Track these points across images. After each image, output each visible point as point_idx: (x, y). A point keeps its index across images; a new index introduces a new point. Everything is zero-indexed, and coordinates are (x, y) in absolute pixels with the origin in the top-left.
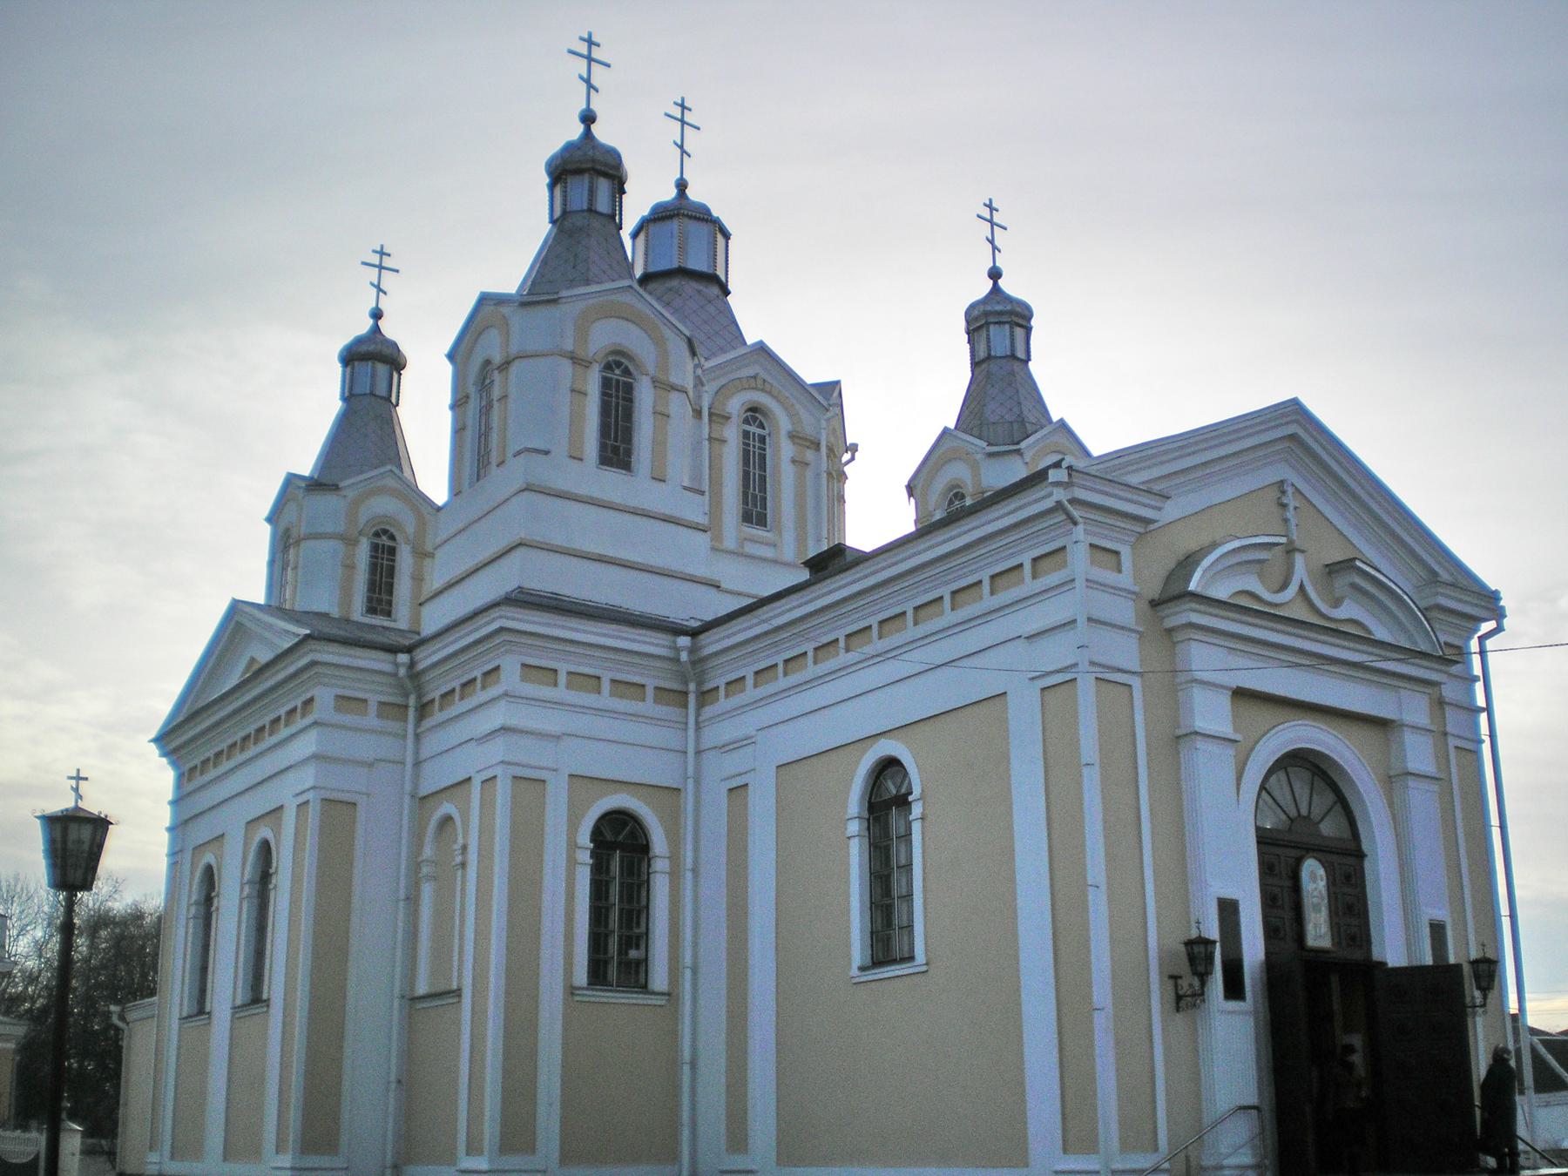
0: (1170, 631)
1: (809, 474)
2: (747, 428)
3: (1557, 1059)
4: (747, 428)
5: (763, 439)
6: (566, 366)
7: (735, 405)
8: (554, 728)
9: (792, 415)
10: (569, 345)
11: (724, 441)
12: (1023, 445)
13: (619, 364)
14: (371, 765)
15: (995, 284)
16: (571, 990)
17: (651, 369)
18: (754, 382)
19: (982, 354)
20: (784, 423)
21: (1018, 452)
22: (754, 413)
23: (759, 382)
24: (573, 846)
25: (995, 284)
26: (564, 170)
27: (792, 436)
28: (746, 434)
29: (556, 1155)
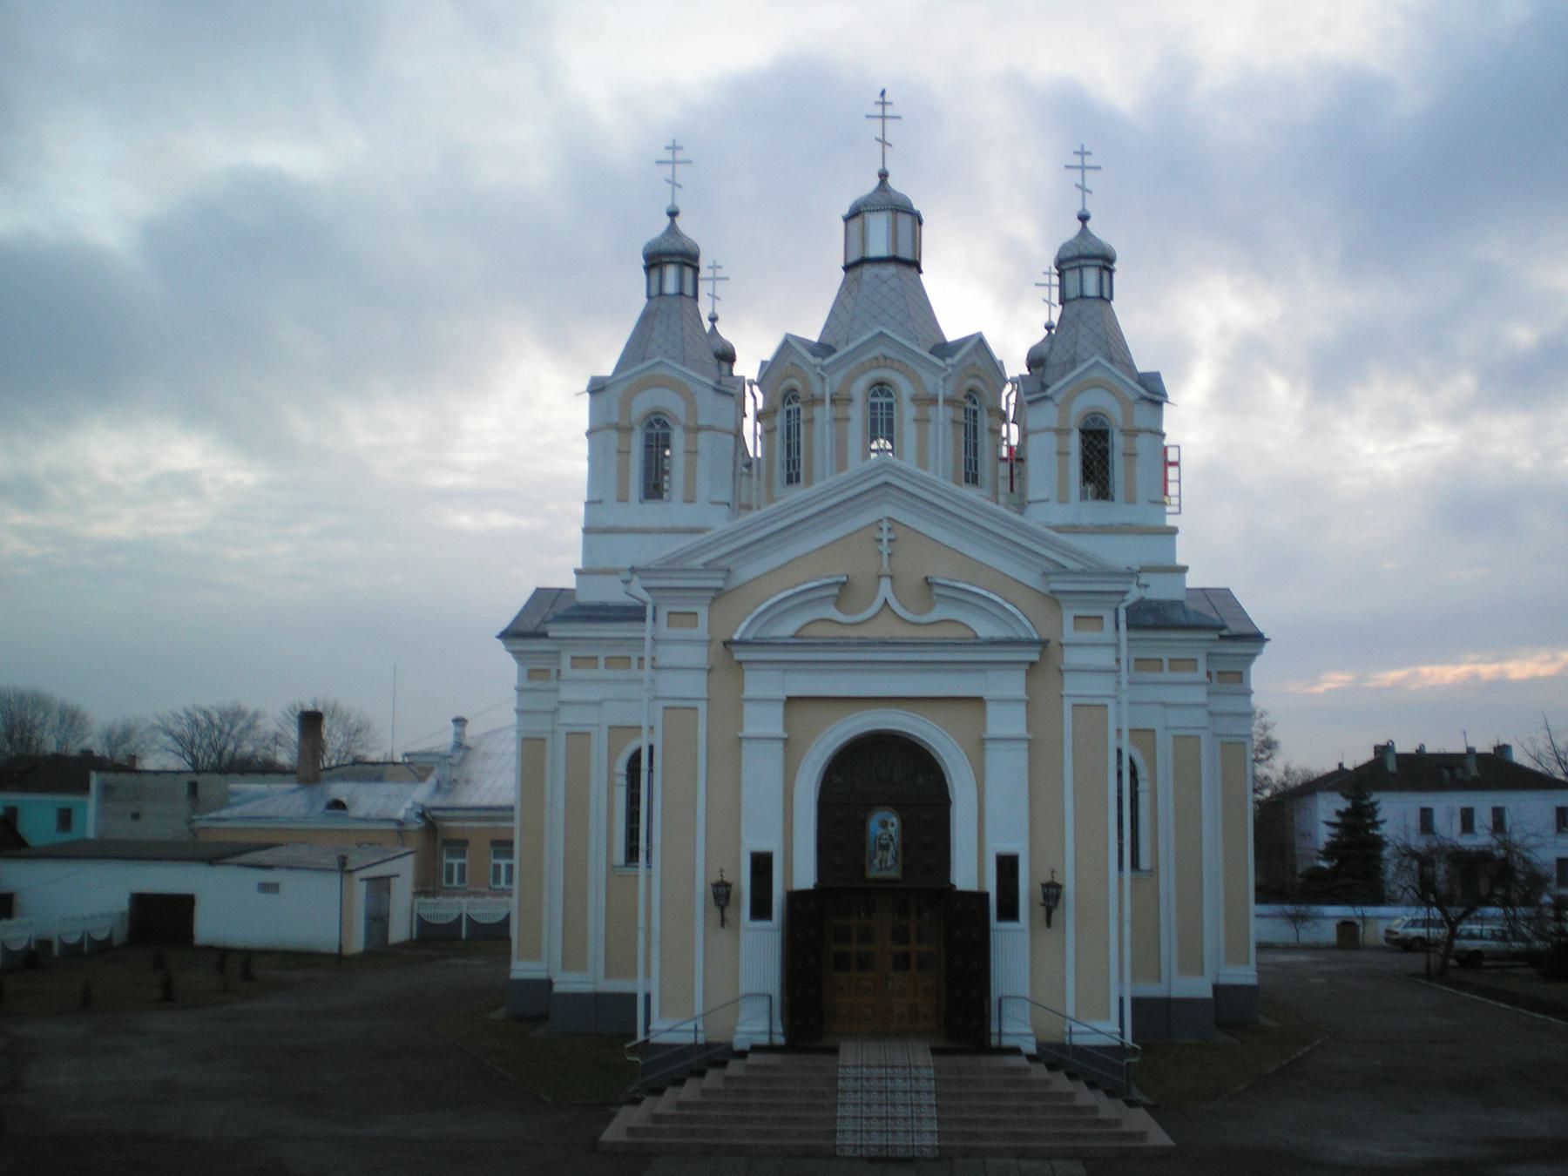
0: (740, 663)
1: (931, 428)
2: (874, 400)
3: (1133, 912)
4: (874, 400)
5: (890, 406)
6: (614, 435)
7: (860, 387)
8: (598, 698)
9: (913, 378)
10: (615, 418)
11: (848, 420)
12: (1049, 392)
13: (658, 421)
14: (599, 703)
15: (1084, 227)
16: (611, 868)
17: (682, 419)
18: (877, 363)
19: (1072, 292)
20: (905, 389)
21: (1046, 398)
22: (880, 387)
23: (881, 360)
24: (611, 774)
25: (1084, 227)
26: (655, 261)
27: (915, 400)
28: (874, 406)
29: (602, 971)
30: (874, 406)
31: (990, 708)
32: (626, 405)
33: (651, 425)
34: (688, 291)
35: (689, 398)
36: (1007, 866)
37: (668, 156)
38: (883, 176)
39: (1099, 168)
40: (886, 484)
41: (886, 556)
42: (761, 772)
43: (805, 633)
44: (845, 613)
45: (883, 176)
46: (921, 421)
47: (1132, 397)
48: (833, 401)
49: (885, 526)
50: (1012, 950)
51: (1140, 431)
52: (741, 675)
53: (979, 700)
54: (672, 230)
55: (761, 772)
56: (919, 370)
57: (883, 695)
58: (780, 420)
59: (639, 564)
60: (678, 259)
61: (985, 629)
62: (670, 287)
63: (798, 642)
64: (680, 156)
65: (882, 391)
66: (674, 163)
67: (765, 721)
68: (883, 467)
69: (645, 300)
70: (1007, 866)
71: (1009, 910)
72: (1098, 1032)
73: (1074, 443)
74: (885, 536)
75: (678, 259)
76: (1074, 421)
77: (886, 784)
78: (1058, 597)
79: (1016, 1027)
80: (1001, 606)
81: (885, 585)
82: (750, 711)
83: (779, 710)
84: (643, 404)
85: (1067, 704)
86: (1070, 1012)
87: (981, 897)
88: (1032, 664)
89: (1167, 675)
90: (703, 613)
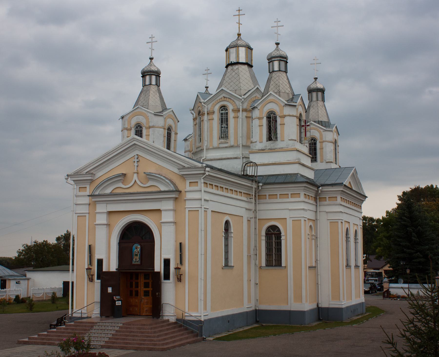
2: (222, 112)
4: (222, 112)
5: (227, 113)
7: (217, 108)
13: (139, 126)
17: (145, 125)
20: (230, 107)
22: (224, 108)
23: (223, 98)
28: (222, 114)
30: (222, 114)
31: (163, 212)
32: (130, 122)
33: (137, 128)
34: (283, 68)
35: (147, 118)
36: (167, 262)
37: (150, 40)
38: (239, 35)
39: (147, 43)
40: (135, 144)
41: (136, 166)
42: (101, 234)
43: (114, 192)
44: (125, 185)
45: (239, 35)
46: (236, 117)
47: (283, 105)
48: (208, 114)
49: (136, 157)
50: (169, 290)
51: (285, 116)
52: (95, 205)
53: (159, 211)
54: (150, 64)
55: (101, 234)
56: (235, 100)
57: (134, 211)
58: (198, 121)
59: (70, 174)
60: (279, 59)
61: (163, 188)
62: (147, 83)
63: (111, 194)
64: (154, 40)
65: (224, 109)
66: (152, 42)
67: (102, 219)
68: (133, 139)
69: (142, 87)
70: (167, 262)
71: (167, 277)
72: (192, 316)
73: (265, 121)
74: (136, 160)
75: (279, 59)
76: (265, 115)
77: (136, 236)
78: (184, 176)
79: (169, 313)
80: (164, 180)
81: (135, 175)
82: (98, 216)
83: (105, 216)
84: (134, 122)
85: (187, 210)
86: (187, 310)
87: (159, 273)
88: (176, 198)
89: (279, 200)
90: (88, 187)
